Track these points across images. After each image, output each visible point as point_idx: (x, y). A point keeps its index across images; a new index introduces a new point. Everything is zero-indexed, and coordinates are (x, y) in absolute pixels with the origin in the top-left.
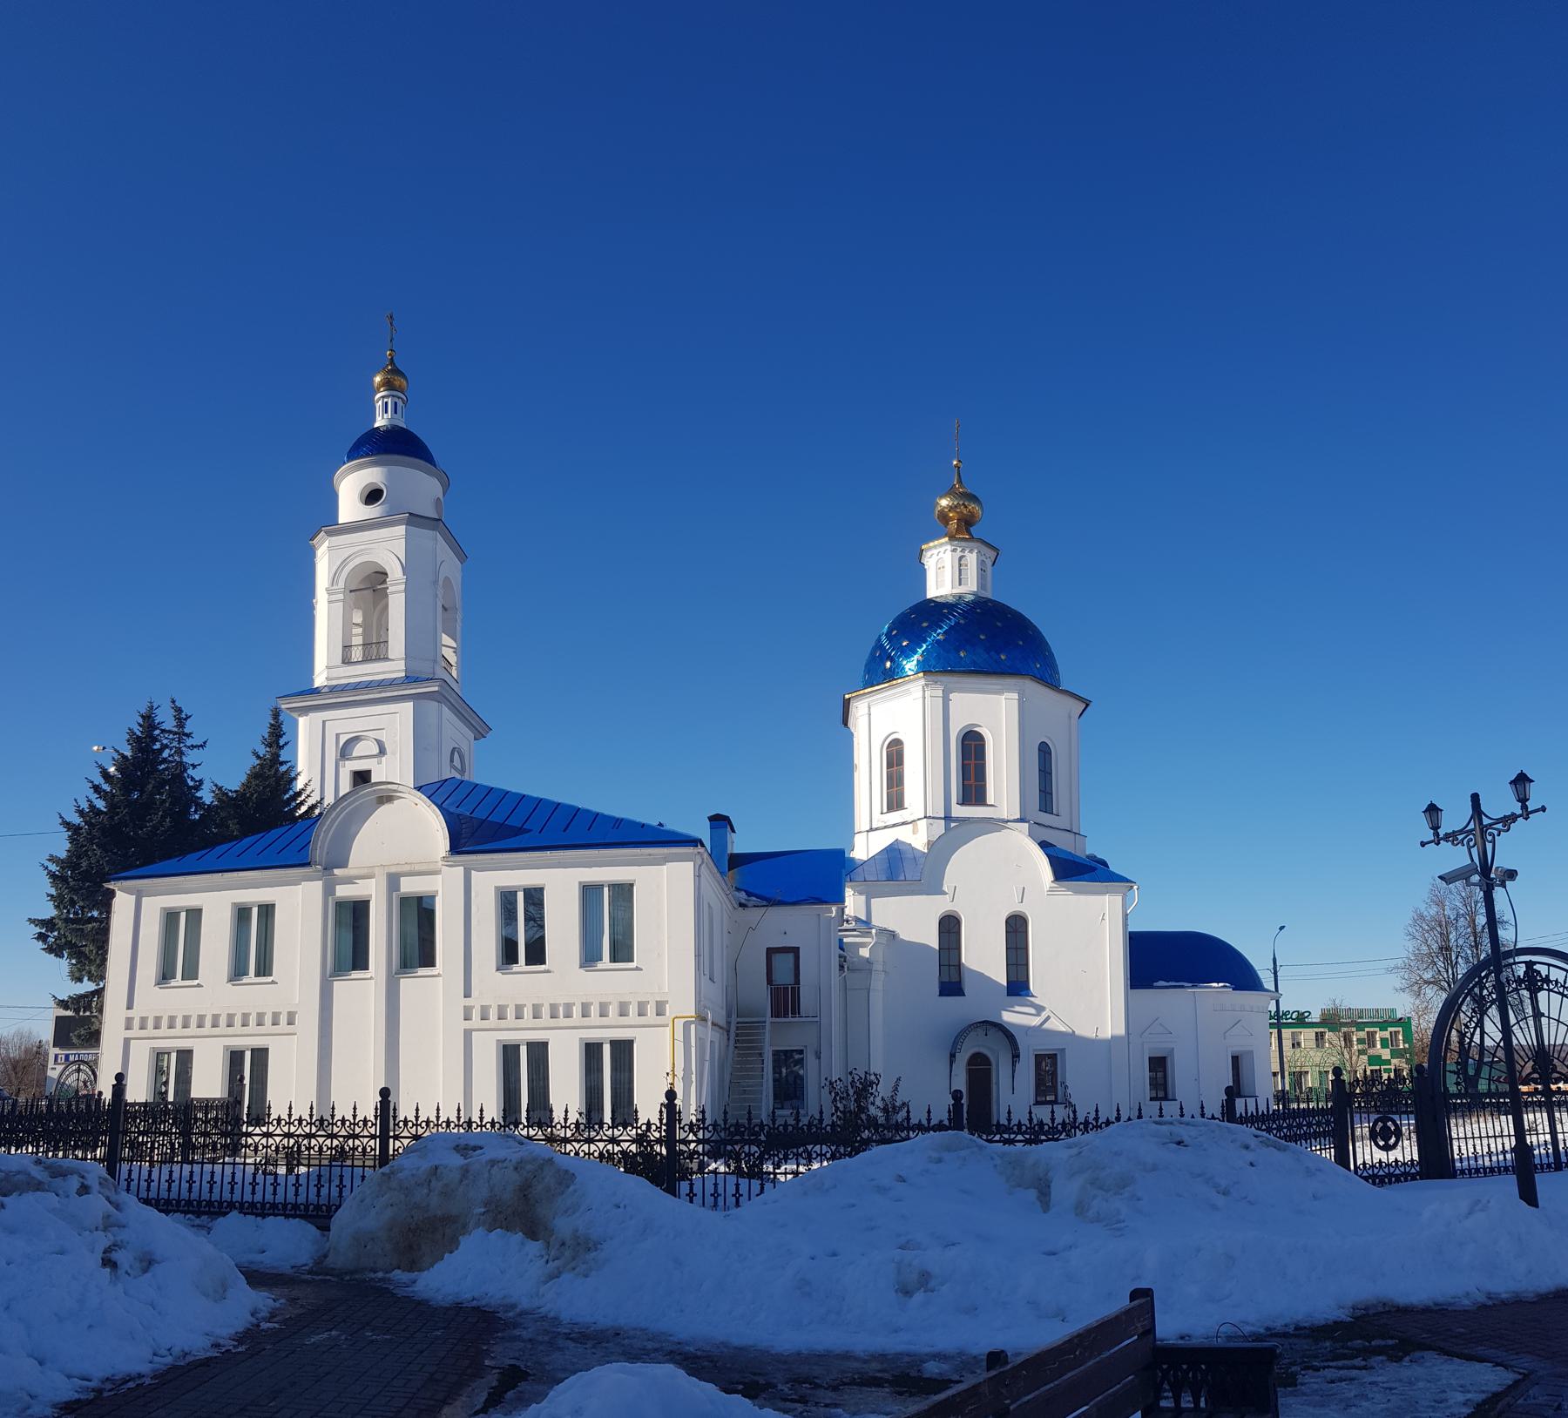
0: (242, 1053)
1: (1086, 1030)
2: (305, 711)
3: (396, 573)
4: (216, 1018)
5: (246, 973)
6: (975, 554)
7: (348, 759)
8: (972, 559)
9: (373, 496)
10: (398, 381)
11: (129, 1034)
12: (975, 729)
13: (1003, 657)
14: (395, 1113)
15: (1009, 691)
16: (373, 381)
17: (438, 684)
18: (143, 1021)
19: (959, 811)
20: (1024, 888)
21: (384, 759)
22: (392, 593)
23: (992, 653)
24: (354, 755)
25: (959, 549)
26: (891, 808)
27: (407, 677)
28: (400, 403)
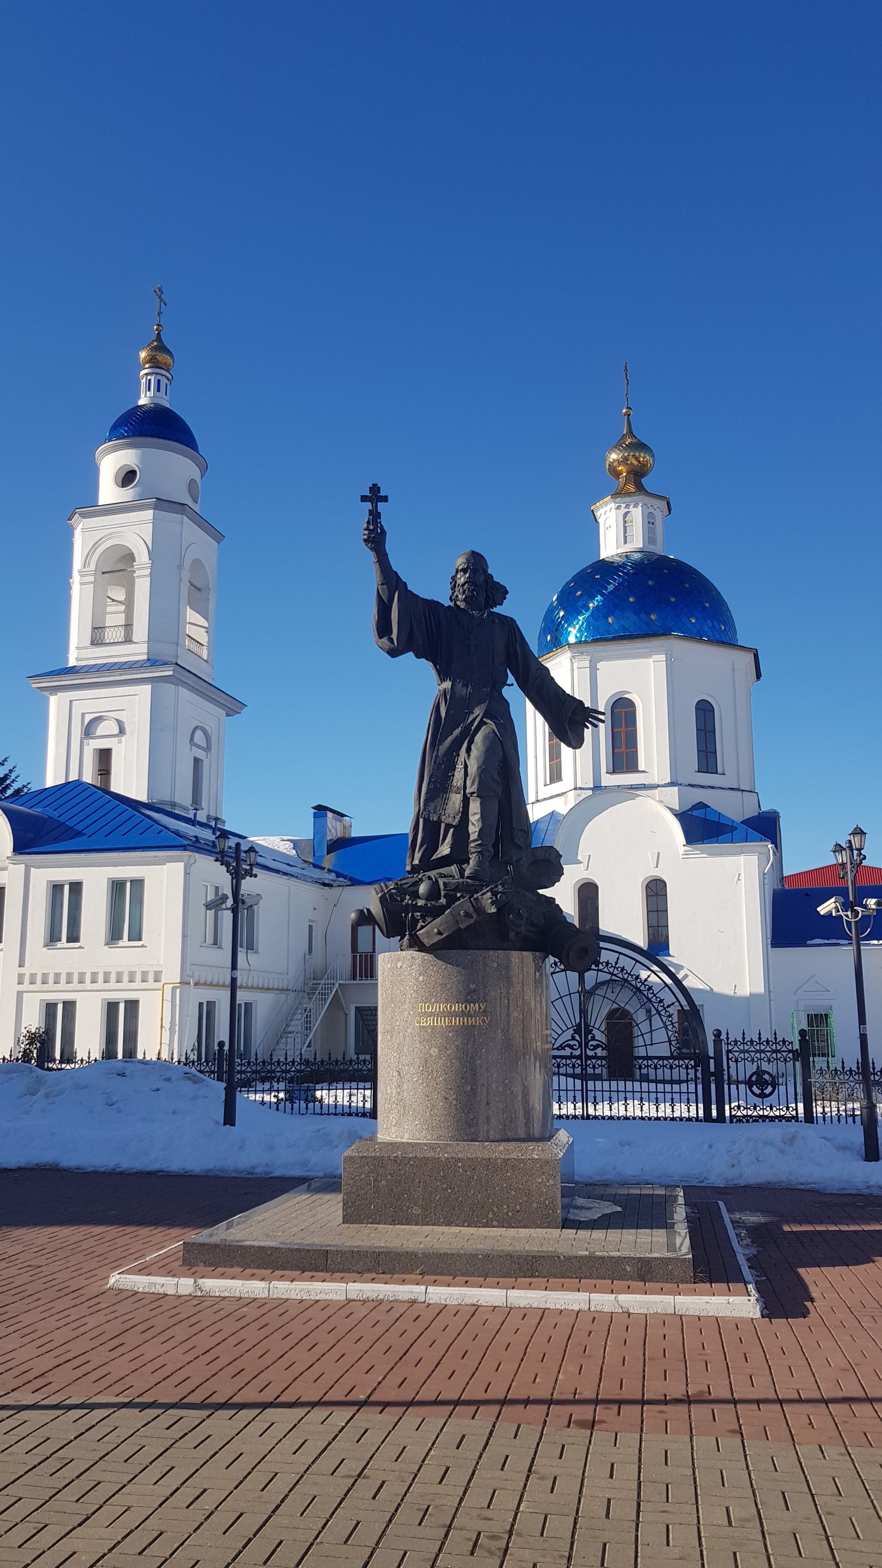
0: (550, 781)
1: (723, 988)
2: (55, 690)
3: (142, 557)
4: (107, 975)
5: (120, 937)
6: (640, 508)
7: (92, 738)
8: (637, 514)
9: (127, 478)
10: (162, 357)
11: (21, 988)
12: (627, 696)
13: (653, 617)
14: (873, 1065)
15: (658, 653)
16: (138, 356)
17: (172, 668)
18: (33, 977)
19: (608, 780)
20: (659, 853)
21: (123, 738)
22: (138, 577)
23: (642, 615)
24: (98, 734)
25: (623, 506)
26: (552, 781)
27: (148, 660)
28: (164, 381)
